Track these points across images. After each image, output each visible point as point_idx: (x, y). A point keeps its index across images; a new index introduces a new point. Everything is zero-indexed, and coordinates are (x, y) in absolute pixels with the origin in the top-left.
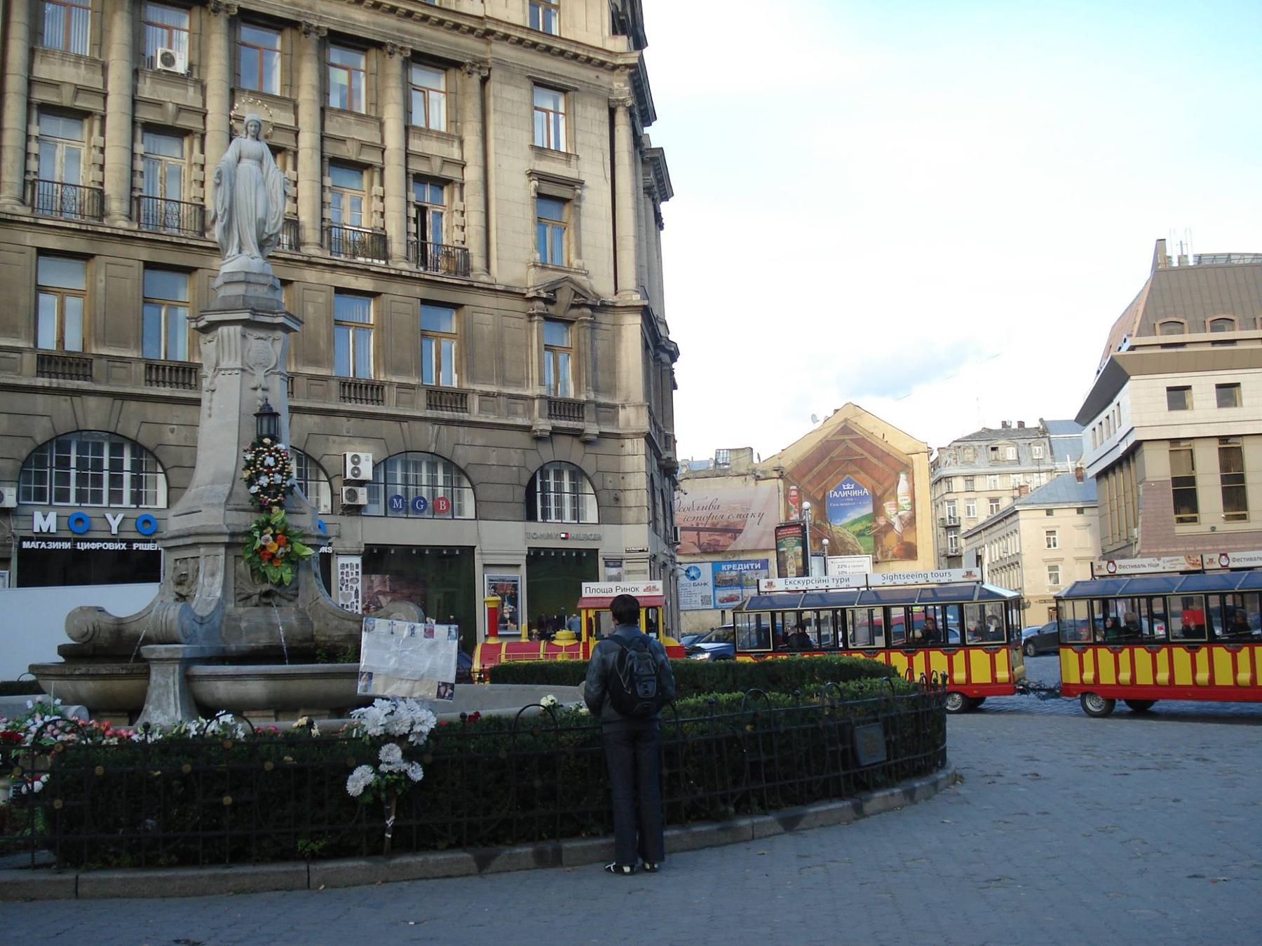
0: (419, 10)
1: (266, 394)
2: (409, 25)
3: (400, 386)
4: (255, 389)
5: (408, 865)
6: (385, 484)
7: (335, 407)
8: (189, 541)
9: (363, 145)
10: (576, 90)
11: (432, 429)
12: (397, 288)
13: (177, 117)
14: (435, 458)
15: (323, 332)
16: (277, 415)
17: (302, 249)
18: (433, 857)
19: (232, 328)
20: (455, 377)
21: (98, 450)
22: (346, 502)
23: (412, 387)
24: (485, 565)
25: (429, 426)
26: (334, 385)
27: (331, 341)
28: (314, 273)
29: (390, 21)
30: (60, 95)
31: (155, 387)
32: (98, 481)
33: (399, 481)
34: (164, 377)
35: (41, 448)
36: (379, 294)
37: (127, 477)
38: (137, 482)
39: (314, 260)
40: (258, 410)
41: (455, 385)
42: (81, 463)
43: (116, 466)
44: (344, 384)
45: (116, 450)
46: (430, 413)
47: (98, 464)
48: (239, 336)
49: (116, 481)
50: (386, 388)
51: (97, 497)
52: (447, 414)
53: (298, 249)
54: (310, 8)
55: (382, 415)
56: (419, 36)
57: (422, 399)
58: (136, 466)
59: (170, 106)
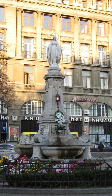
0: (48, 3)
1: (58, 92)
2: (96, 14)
3: (96, 89)
4: (56, 91)
5: (72, 191)
6: (93, 109)
7: (83, 94)
8: (43, 122)
9: (105, 42)
10: (7, 6)
11: (103, 98)
12: (95, 69)
13: (30, 35)
14: (104, 104)
15: (80, 78)
16: (60, 96)
17: (75, 62)
18: (78, 189)
19: (51, 79)
20: (108, 87)
21: (100, 106)
22: (85, 113)
23: (99, 89)
24: (9, 125)
25: (102, 97)
26: (82, 89)
27: (82, 80)
28: (78, 67)
29: (92, 14)
30: (28, 34)
31: (70, 92)
32: (100, 112)
33: (96, 109)
34: (86, 91)
35: (26, 103)
36: (91, 70)
37: (105, 111)
38: (107, 112)
39: (77, 64)
40: (56, 95)
41: (108, 89)
42: (98, 108)
43: (103, 109)
44: (85, 89)
45: (103, 106)
46: (102, 95)
47: (100, 109)
48: (52, 80)
49: (103, 112)
50: (93, 90)
51: (100, 115)
52: (106, 95)
53: (74, 62)
54: (76, 13)
55: (92, 95)
56: (98, 17)
57: (101, 92)
58: (106, 109)
59: (49, 35)
